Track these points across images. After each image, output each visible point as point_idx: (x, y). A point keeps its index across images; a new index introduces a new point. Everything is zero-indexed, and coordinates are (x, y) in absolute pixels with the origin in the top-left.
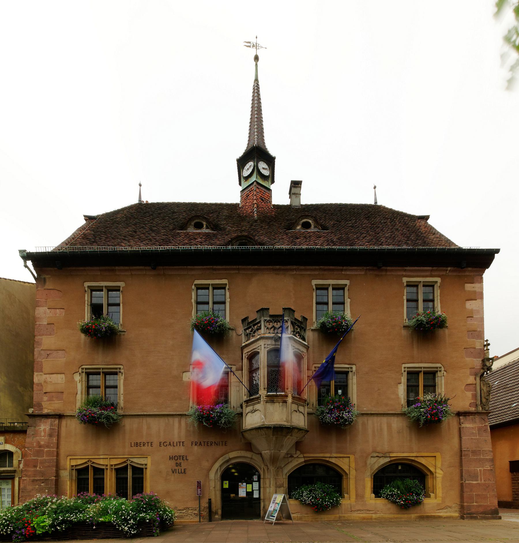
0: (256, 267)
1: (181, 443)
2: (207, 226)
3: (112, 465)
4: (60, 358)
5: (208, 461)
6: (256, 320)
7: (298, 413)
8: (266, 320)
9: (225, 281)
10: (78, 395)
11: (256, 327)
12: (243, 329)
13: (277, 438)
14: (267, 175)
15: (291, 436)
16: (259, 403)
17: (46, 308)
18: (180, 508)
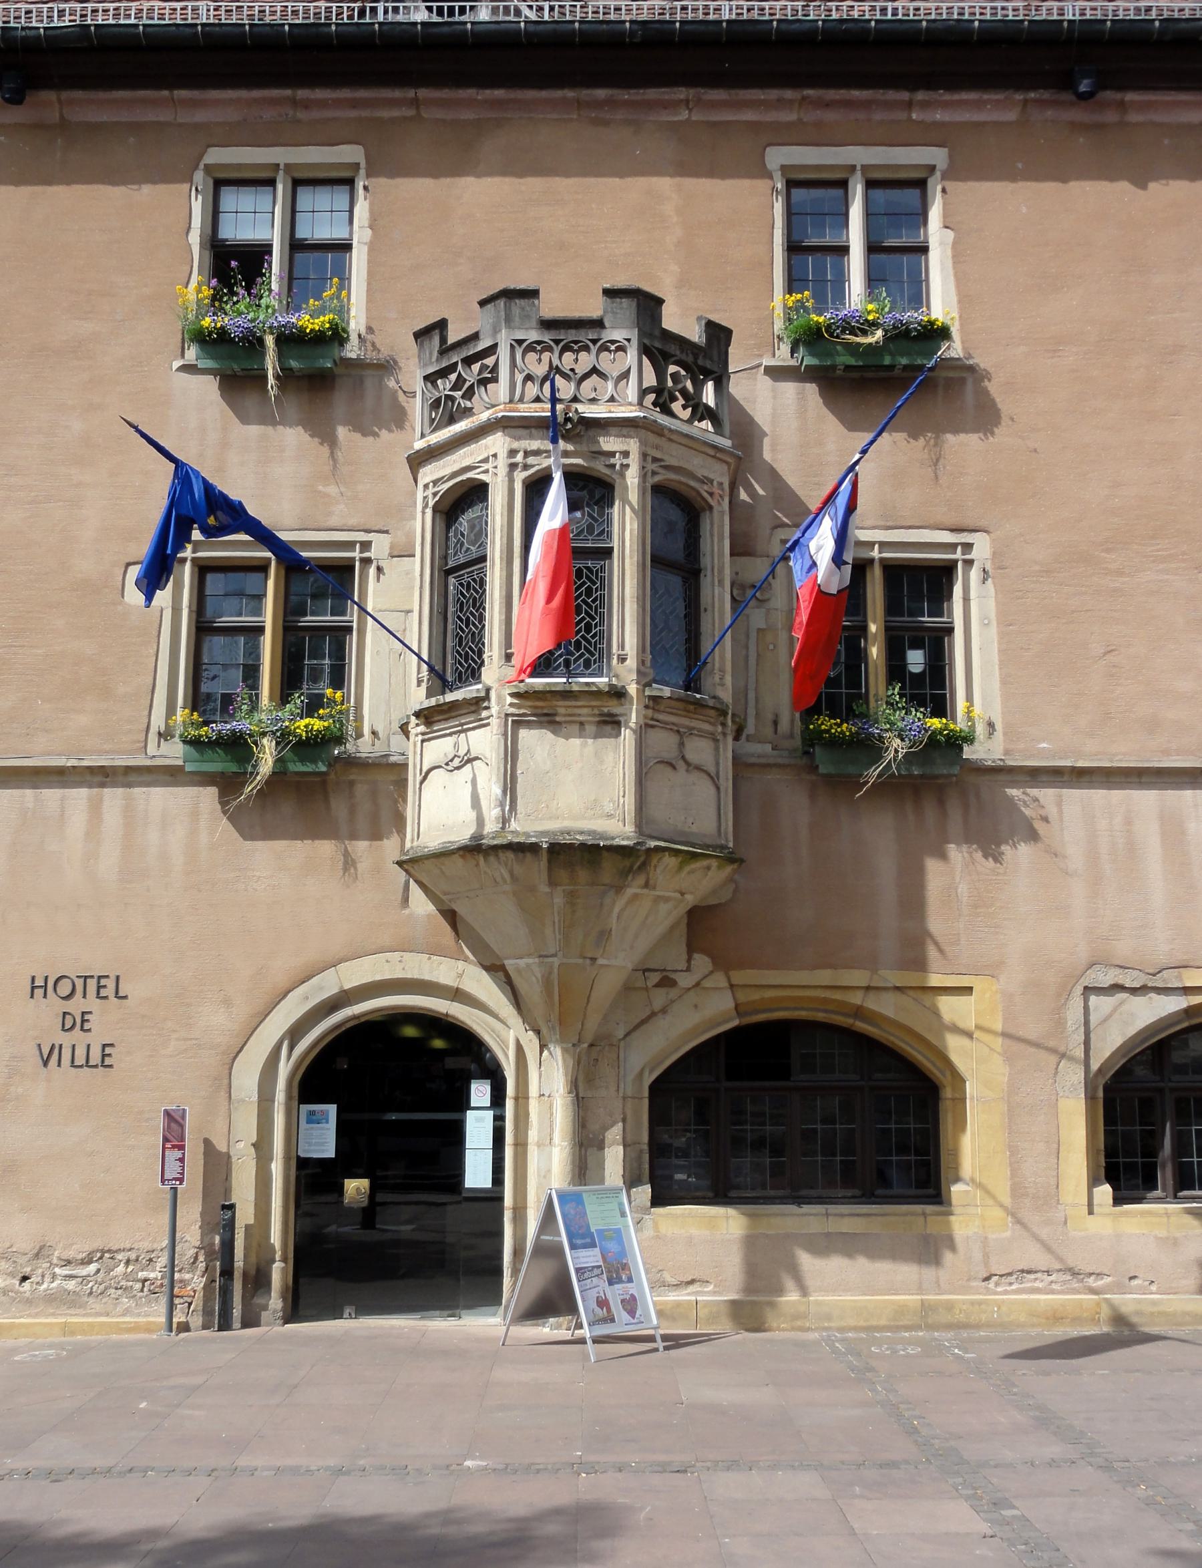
5: (227, 1002)
6: (475, 337)
7: (681, 775)
8: (520, 342)
9: (350, 153)
11: (476, 367)
12: (419, 375)
13: (571, 896)
15: (646, 885)
18: (70, 1254)
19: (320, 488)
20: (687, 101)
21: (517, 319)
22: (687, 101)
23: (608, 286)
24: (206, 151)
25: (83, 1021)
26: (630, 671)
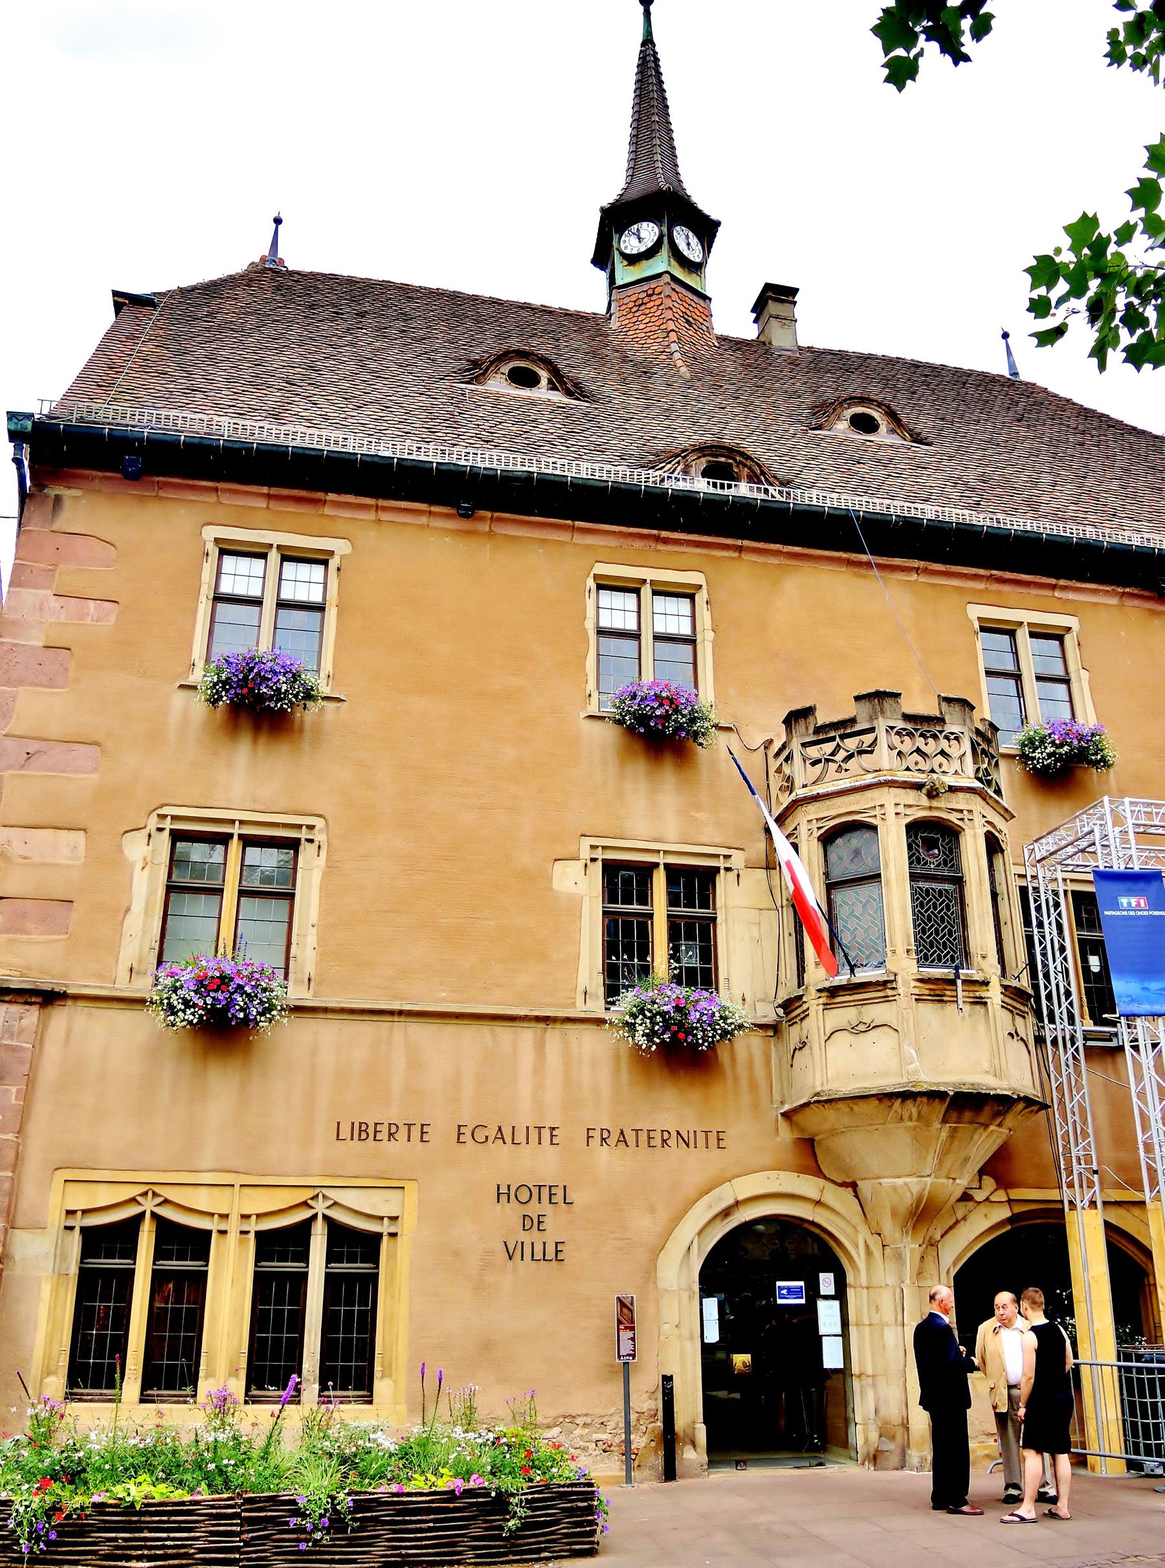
0: (797, 549)
1: (546, 1134)
2: (550, 381)
3: (245, 1217)
4: (76, 771)
5: (652, 1210)
6: (853, 721)
8: (892, 728)
10: (130, 918)
13: (954, 1132)
16: (886, 999)
17: (49, 593)
25: (539, 1222)
26: (991, 966)
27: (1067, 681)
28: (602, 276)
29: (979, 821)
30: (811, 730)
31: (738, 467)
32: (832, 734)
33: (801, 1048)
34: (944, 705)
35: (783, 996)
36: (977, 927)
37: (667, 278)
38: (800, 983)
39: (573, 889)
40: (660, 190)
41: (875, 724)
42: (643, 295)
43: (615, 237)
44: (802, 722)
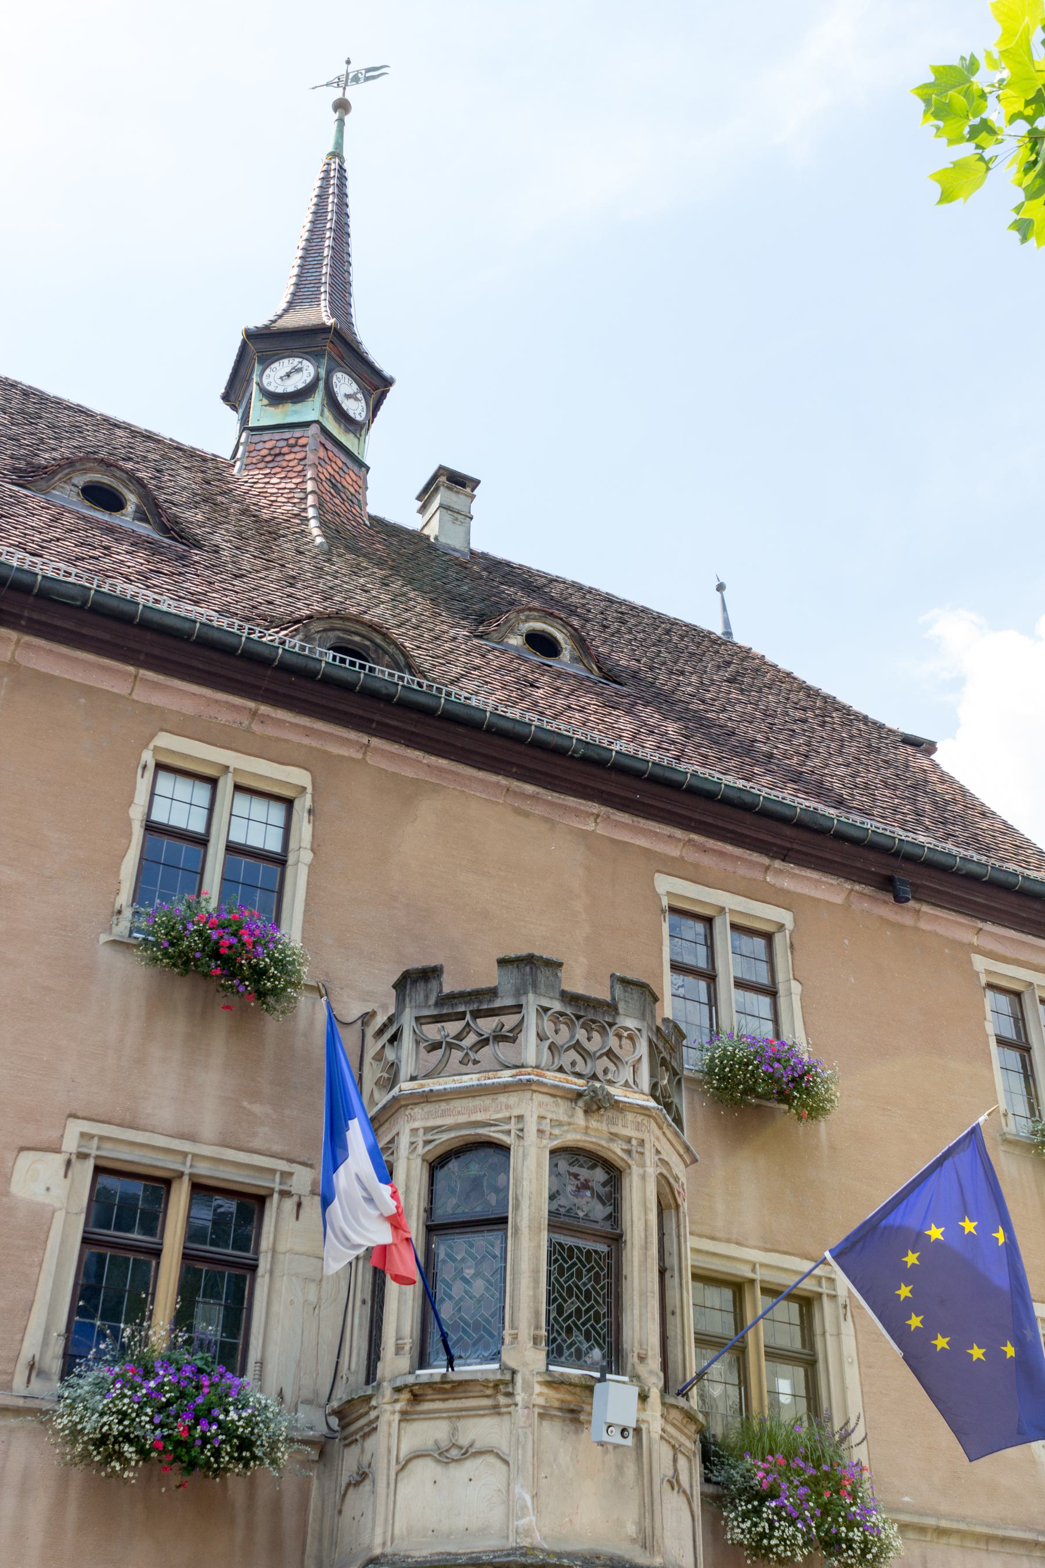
6: (492, 993)
8: (546, 1010)
14: (358, 418)
16: (496, 1410)
19: (245, 1104)
20: (598, 816)
21: (543, 986)
22: (598, 816)
23: (502, 956)
24: (156, 734)
26: (651, 1372)
27: (771, 992)
28: (232, 418)
29: (650, 1157)
30: (432, 1000)
31: (376, 651)
32: (461, 1009)
33: (357, 1484)
34: (618, 988)
35: (341, 1395)
36: (636, 1312)
37: (314, 429)
38: (371, 1376)
39: (41, 1197)
40: (324, 324)
41: (523, 1000)
42: (284, 443)
43: (257, 368)
44: (421, 986)
